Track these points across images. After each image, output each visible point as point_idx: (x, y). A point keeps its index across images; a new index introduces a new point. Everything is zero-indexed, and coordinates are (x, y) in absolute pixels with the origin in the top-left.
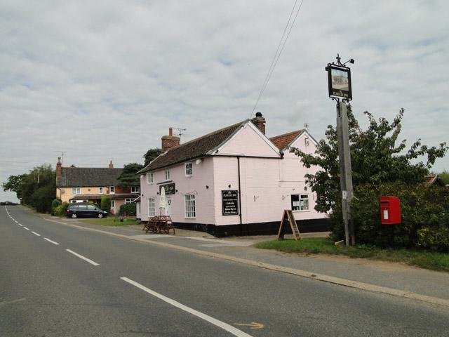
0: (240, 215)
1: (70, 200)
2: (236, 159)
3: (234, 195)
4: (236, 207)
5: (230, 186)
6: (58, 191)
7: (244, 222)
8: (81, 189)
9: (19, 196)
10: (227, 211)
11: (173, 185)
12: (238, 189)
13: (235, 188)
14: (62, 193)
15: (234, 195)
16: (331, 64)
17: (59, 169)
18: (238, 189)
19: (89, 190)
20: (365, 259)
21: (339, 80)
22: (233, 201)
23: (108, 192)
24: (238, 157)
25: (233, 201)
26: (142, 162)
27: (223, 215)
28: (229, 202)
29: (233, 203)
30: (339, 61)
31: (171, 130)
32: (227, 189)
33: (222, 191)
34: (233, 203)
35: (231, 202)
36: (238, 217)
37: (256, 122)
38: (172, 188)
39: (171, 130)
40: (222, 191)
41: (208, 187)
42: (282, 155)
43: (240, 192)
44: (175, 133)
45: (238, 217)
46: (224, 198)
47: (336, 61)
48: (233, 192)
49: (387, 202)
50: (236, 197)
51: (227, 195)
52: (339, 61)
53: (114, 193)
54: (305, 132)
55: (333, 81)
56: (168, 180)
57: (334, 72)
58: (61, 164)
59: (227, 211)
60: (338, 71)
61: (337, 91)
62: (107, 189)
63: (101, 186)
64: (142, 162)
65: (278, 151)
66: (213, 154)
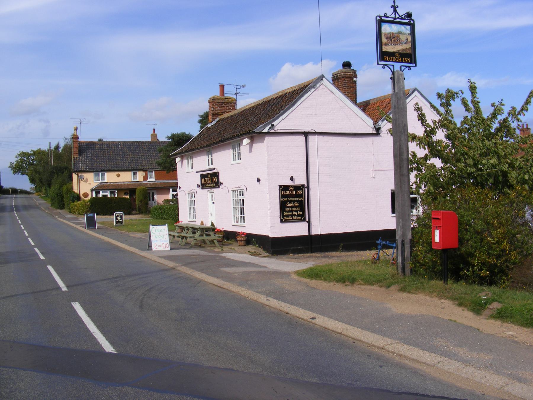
0: (309, 222)
1: (92, 191)
2: (302, 138)
3: (299, 192)
4: (302, 209)
5: (292, 179)
6: (75, 177)
7: (314, 232)
8: (106, 174)
9: (32, 181)
10: (287, 216)
11: (217, 175)
12: (305, 183)
13: (300, 180)
14: (80, 179)
15: (299, 192)
16: (380, 17)
17: (76, 144)
18: (305, 183)
19: (118, 176)
20: (375, 287)
21: (394, 38)
22: (297, 201)
23: (145, 178)
24: (306, 134)
25: (297, 201)
26: (194, 130)
27: (282, 221)
28: (290, 202)
29: (296, 204)
30: (395, 11)
31: (222, 87)
32: (289, 183)
33: (280, 186)
34: (296, 204)
35: (294, 202)
36: (305, 224)
37: (336, 80)
38: (215, 179)
39: (222, 87)
40: (280, 186)
41: (259, 180)
42: (378, 129)
43: (308, 187)
44: (229, 93)
45: (305, 224)
46: (282, 196)
47: (390, 12)
48: (298, 188)
49: (438, 219)
50: (302, 195)
51: (288, 192)
52: (395, 11)
53: (153, 179)
54: (416, 93)
55: (384, 40)
56: (211, 167)
57: (387, 29)
58: (78, 138)
59: (287, 216)
60: (393, 26)
61: (391, 55)
62: (144, 174)
63: (134, 171)
64: (194, 130)
65: (371, 122)
66: (266, 130)
